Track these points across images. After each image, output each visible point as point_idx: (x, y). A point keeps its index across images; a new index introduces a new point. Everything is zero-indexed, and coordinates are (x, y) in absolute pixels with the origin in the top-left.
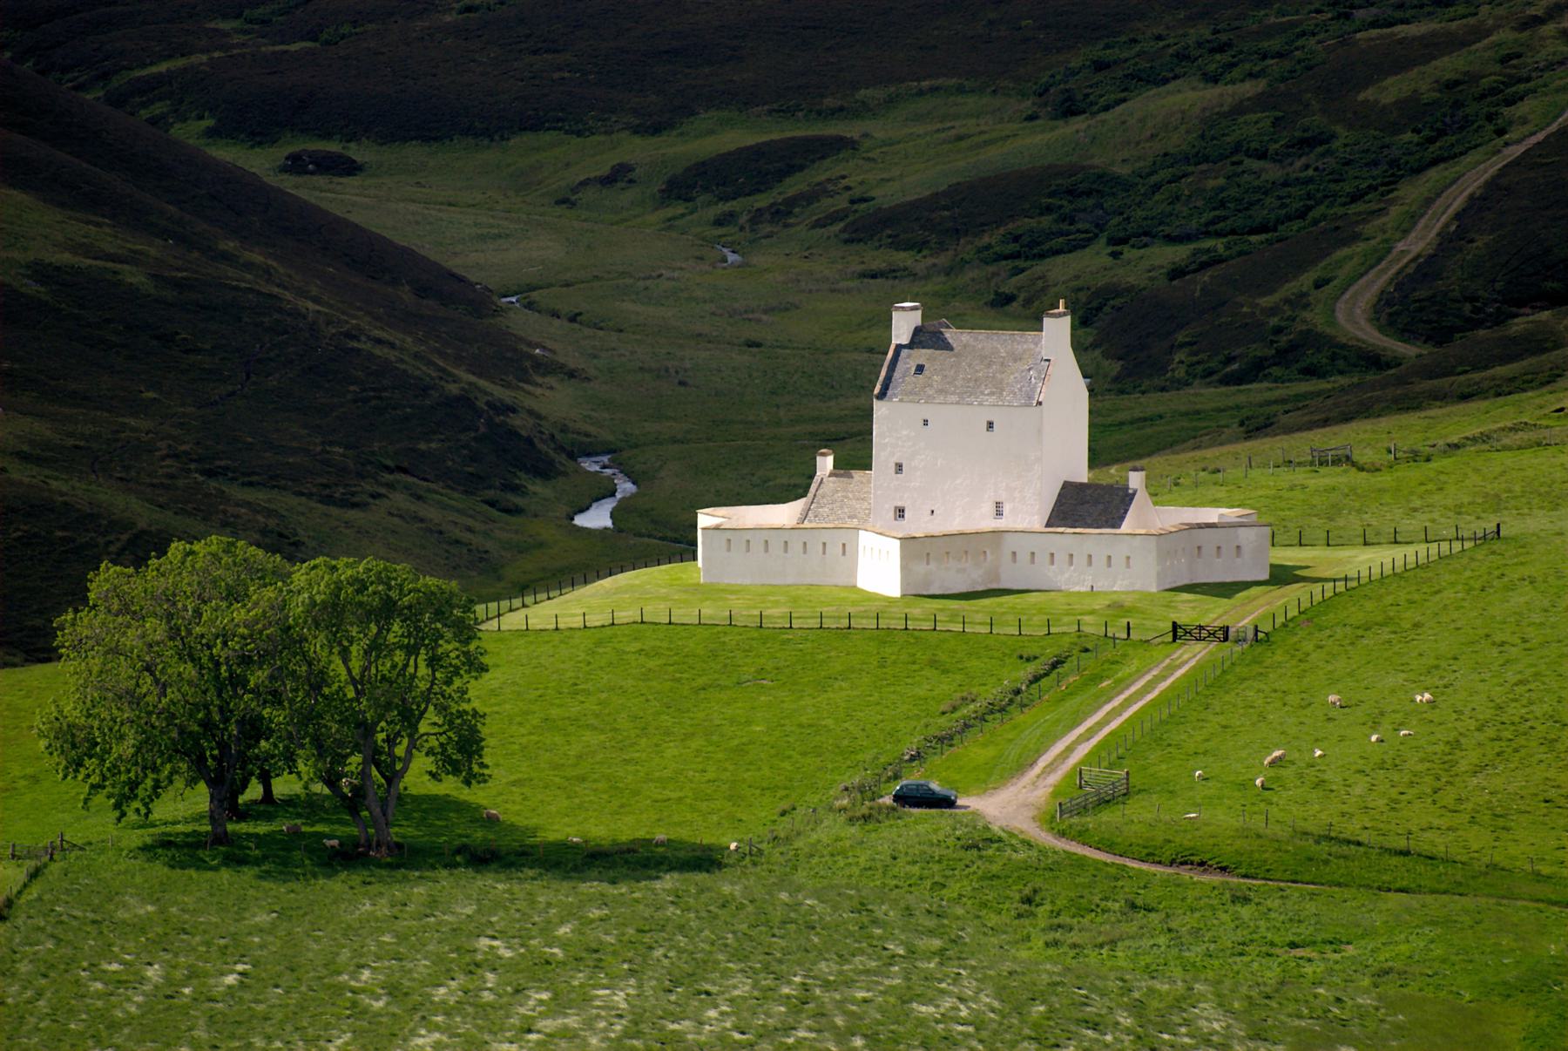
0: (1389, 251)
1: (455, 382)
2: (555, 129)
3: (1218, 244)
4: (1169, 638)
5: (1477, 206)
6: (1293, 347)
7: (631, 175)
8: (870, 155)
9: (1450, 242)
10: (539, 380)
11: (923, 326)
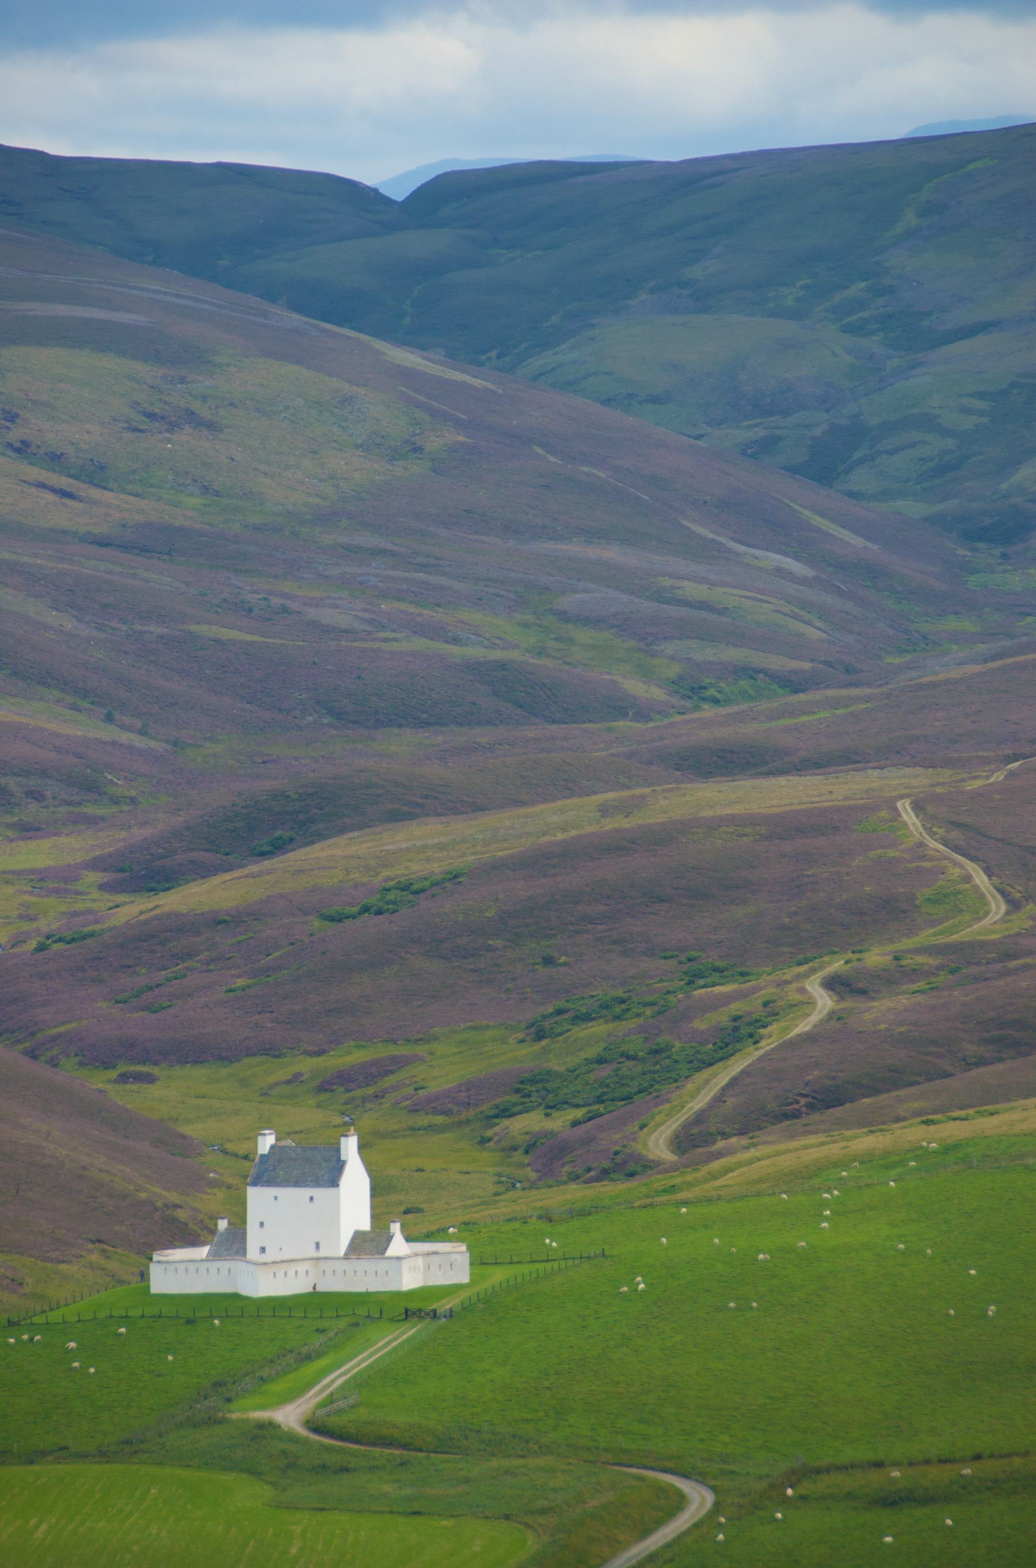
0: (683, 1107)
1: (145, 1192)
2: (265, 1055)
3: (601, 1108)
4: (404, 1316)
5: (734, 1082)
6: (624, 1163)
7: (301, 1079)
8: (431, 1063)
9: (719, 1099)
10: (209, 1191)
11: (275, 1144)
